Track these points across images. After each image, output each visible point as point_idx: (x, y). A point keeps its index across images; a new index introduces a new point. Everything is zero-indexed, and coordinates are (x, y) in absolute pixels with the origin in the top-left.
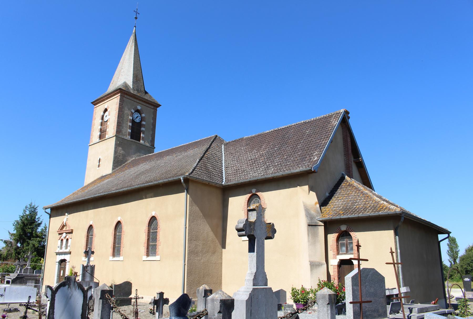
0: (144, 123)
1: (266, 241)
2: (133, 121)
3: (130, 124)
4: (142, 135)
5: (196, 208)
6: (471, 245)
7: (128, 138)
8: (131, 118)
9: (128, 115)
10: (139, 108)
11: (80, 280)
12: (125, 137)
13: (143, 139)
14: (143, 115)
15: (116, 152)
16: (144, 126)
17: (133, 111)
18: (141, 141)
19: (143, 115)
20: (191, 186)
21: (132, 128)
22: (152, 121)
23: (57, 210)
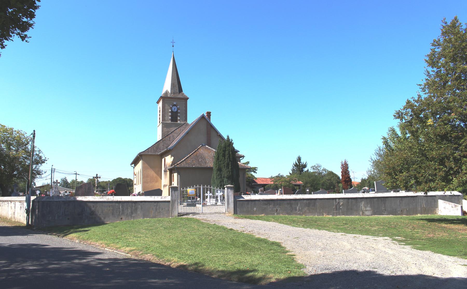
0: (179, 111)
1: (170, 200)
2: (172, 112)
3: (170, 114)
4: (178, 118)
5: (147, 165)
6: (14, 43)
7: (170, 122)
8: (170, 110)
9: (168, 109)
10: (175, 103)
11: (23, 20)
12: (167, 122)
13: (179, 120)
14: (178, 107)
15: (162, 131)
16: (179, 113)
17: (171, 106)
18: (179, 122)
19: (178, 107)
20: (143, 157)
21: (171, 116)
22: (184, 109)
23: (462, 207)
